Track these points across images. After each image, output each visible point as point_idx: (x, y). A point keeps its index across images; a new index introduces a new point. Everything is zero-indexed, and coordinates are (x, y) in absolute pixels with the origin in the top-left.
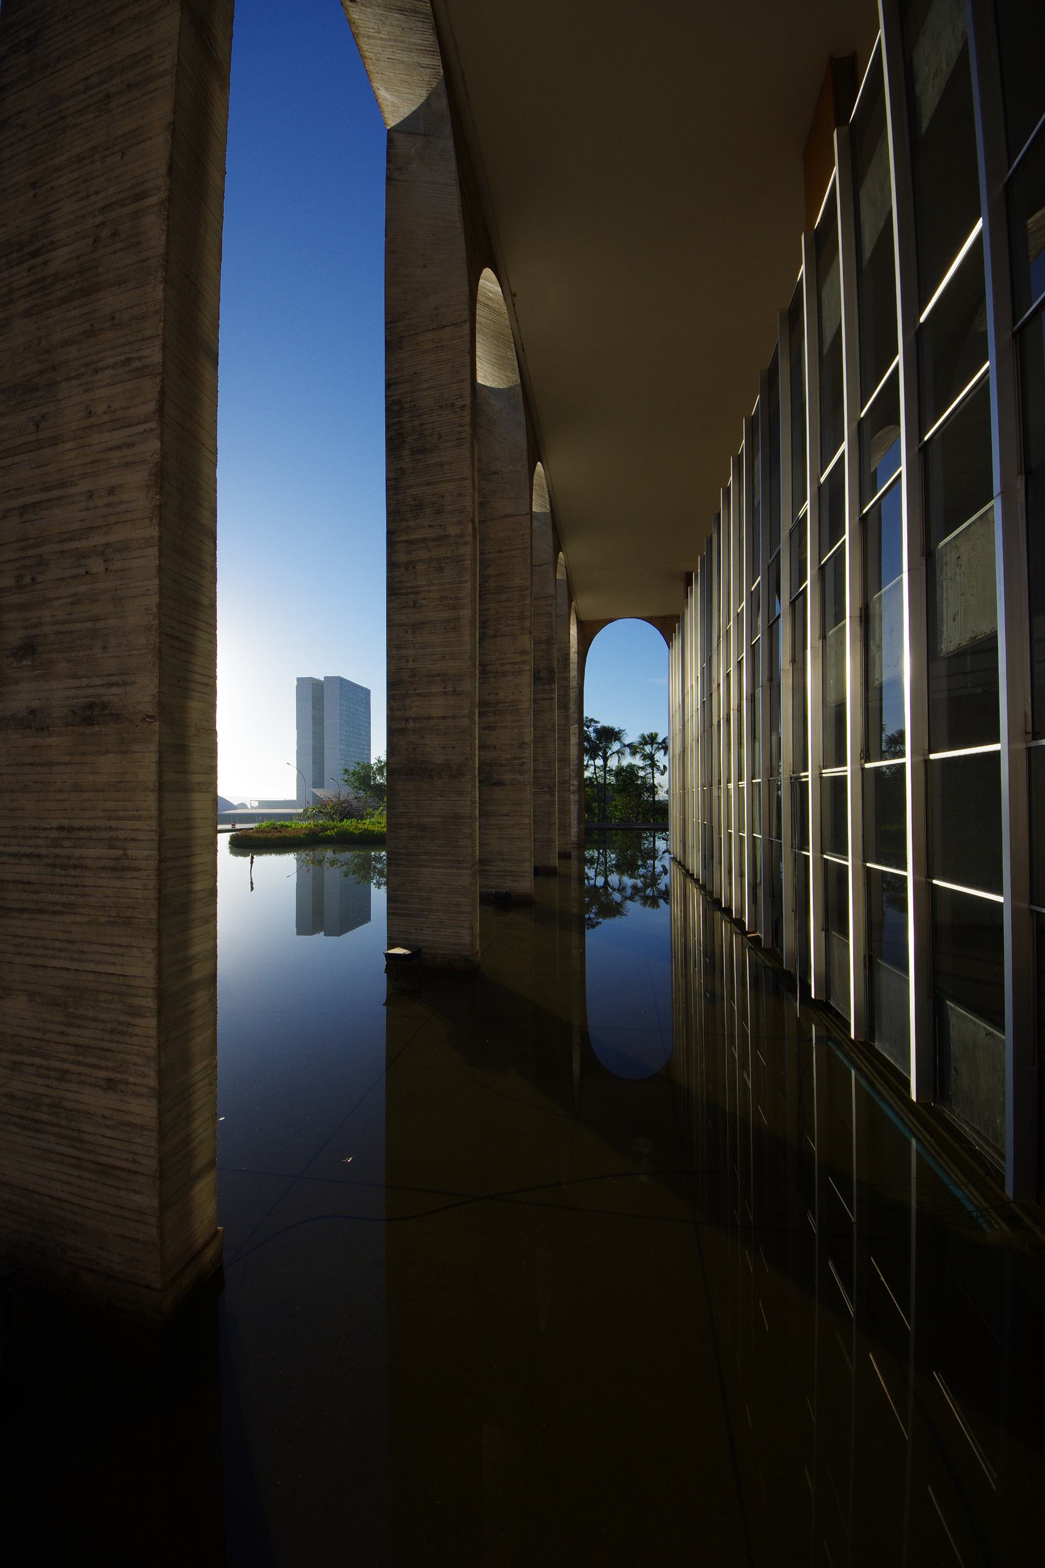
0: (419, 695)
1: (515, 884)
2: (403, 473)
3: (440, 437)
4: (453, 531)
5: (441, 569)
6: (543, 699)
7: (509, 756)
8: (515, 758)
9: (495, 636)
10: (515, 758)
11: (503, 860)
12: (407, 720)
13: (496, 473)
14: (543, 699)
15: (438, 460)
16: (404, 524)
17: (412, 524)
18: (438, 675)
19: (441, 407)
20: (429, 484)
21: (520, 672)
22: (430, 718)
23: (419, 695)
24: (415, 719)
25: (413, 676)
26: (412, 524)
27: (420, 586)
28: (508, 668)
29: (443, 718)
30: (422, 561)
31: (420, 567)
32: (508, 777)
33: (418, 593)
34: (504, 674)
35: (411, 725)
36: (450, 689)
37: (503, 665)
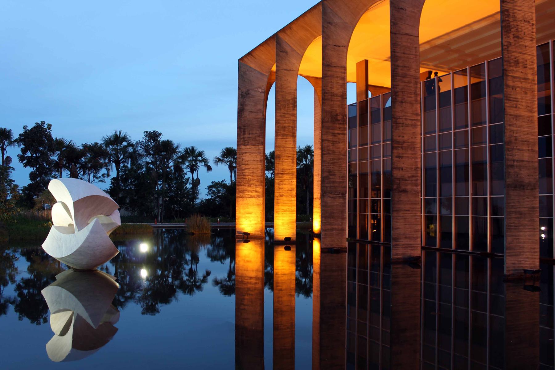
0: (518, 149)
1: (412, 252)
2: (510, 45)
3: (524, 34)
4: (530, 77)
5: (526, 93)
6: (339, 134)
7: (410, 175)
8: (413, 176)
9: (402, 102)
10: (413, 176)
11: (406, 238)
12: (514, 161)
13: (402, 9)
14: (339, 134)
15: (524, 44)
16: (511, 68)
17: (514, 69)
18: (526, 141)
19: (524, 21)
20: (521, 53)
21: (415, 126)
22: (523, 161)
23: (518, 149)
24: (517, 161)
25: (516, 140)
26: (514, 69)
27: (517, 99)
28: (409, 122)
29: (528, 162)
30: (519, 87)
31: (518, 89)
32: (409, 187)
33: (518, 101)
34: (407, 125)
35: (516, 163)
36: (530, 148)
37: (406, 119)
